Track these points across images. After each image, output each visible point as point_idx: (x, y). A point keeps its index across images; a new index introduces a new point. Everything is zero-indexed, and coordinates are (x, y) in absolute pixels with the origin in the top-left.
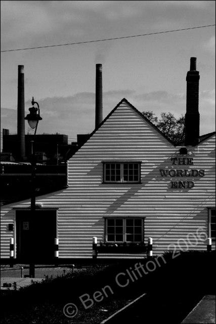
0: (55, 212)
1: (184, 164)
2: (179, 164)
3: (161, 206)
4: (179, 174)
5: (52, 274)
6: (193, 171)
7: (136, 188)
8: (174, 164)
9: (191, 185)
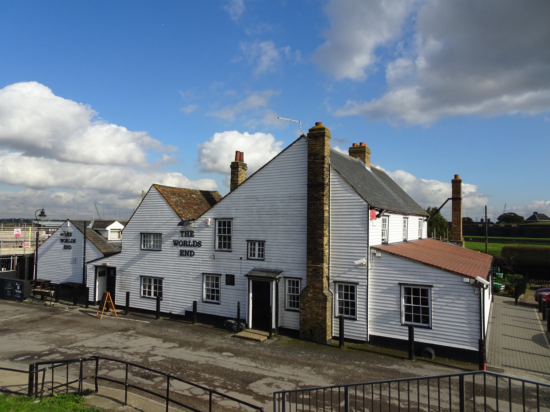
0: (162, 280)
1: (188, 236)
2: (185, 236)
3: (343, 213)
4: (185, 244)
5: (288, 367)
6: (194, 242)
7: (145, 253)
8: (182, 236)
9: (192, 253)
